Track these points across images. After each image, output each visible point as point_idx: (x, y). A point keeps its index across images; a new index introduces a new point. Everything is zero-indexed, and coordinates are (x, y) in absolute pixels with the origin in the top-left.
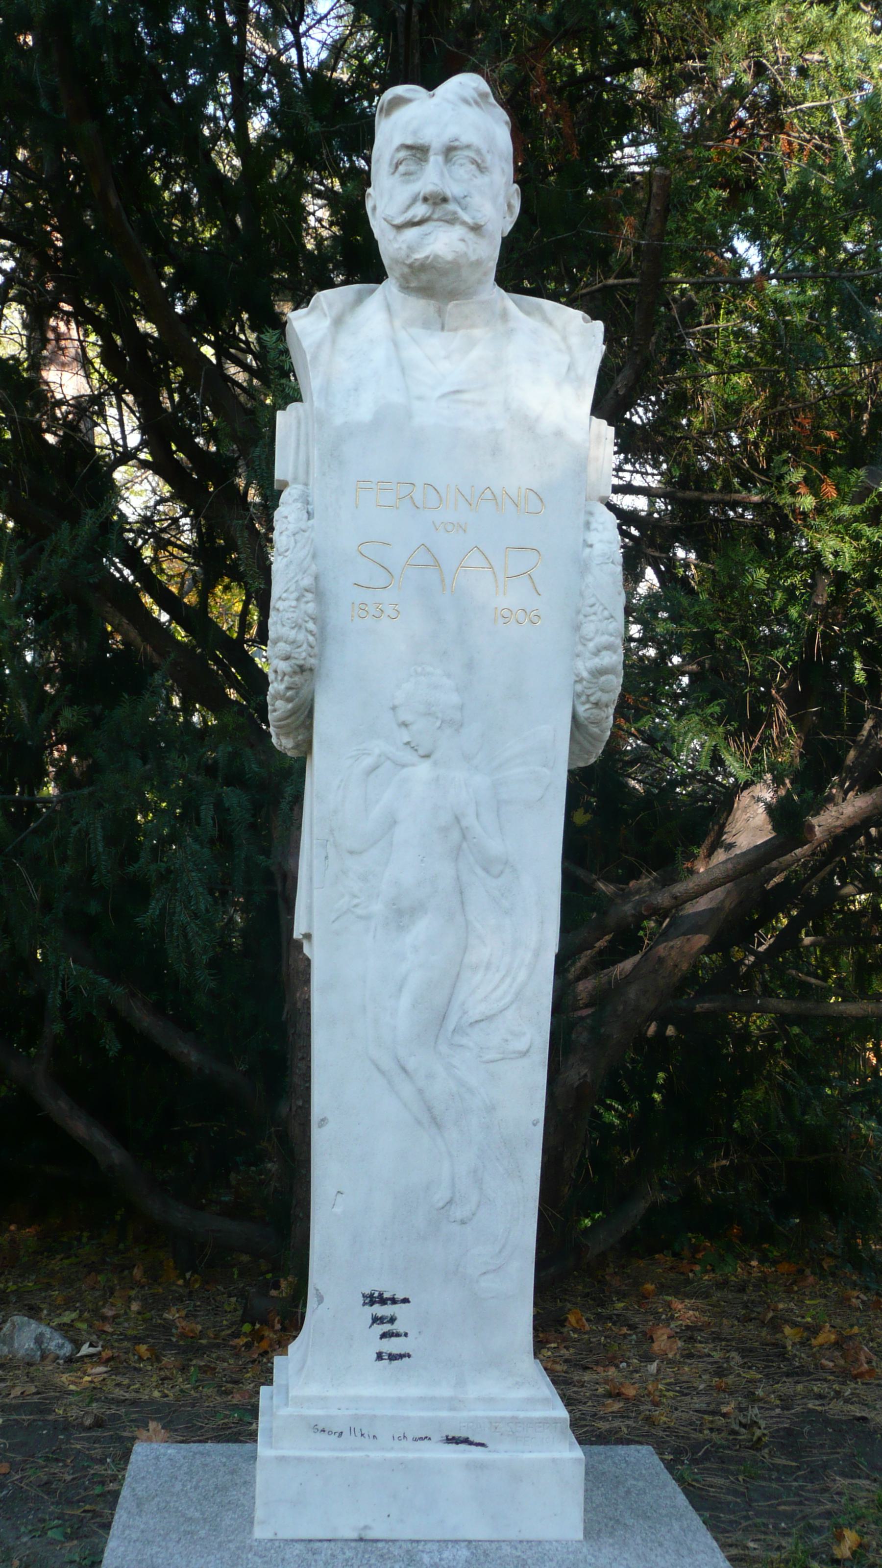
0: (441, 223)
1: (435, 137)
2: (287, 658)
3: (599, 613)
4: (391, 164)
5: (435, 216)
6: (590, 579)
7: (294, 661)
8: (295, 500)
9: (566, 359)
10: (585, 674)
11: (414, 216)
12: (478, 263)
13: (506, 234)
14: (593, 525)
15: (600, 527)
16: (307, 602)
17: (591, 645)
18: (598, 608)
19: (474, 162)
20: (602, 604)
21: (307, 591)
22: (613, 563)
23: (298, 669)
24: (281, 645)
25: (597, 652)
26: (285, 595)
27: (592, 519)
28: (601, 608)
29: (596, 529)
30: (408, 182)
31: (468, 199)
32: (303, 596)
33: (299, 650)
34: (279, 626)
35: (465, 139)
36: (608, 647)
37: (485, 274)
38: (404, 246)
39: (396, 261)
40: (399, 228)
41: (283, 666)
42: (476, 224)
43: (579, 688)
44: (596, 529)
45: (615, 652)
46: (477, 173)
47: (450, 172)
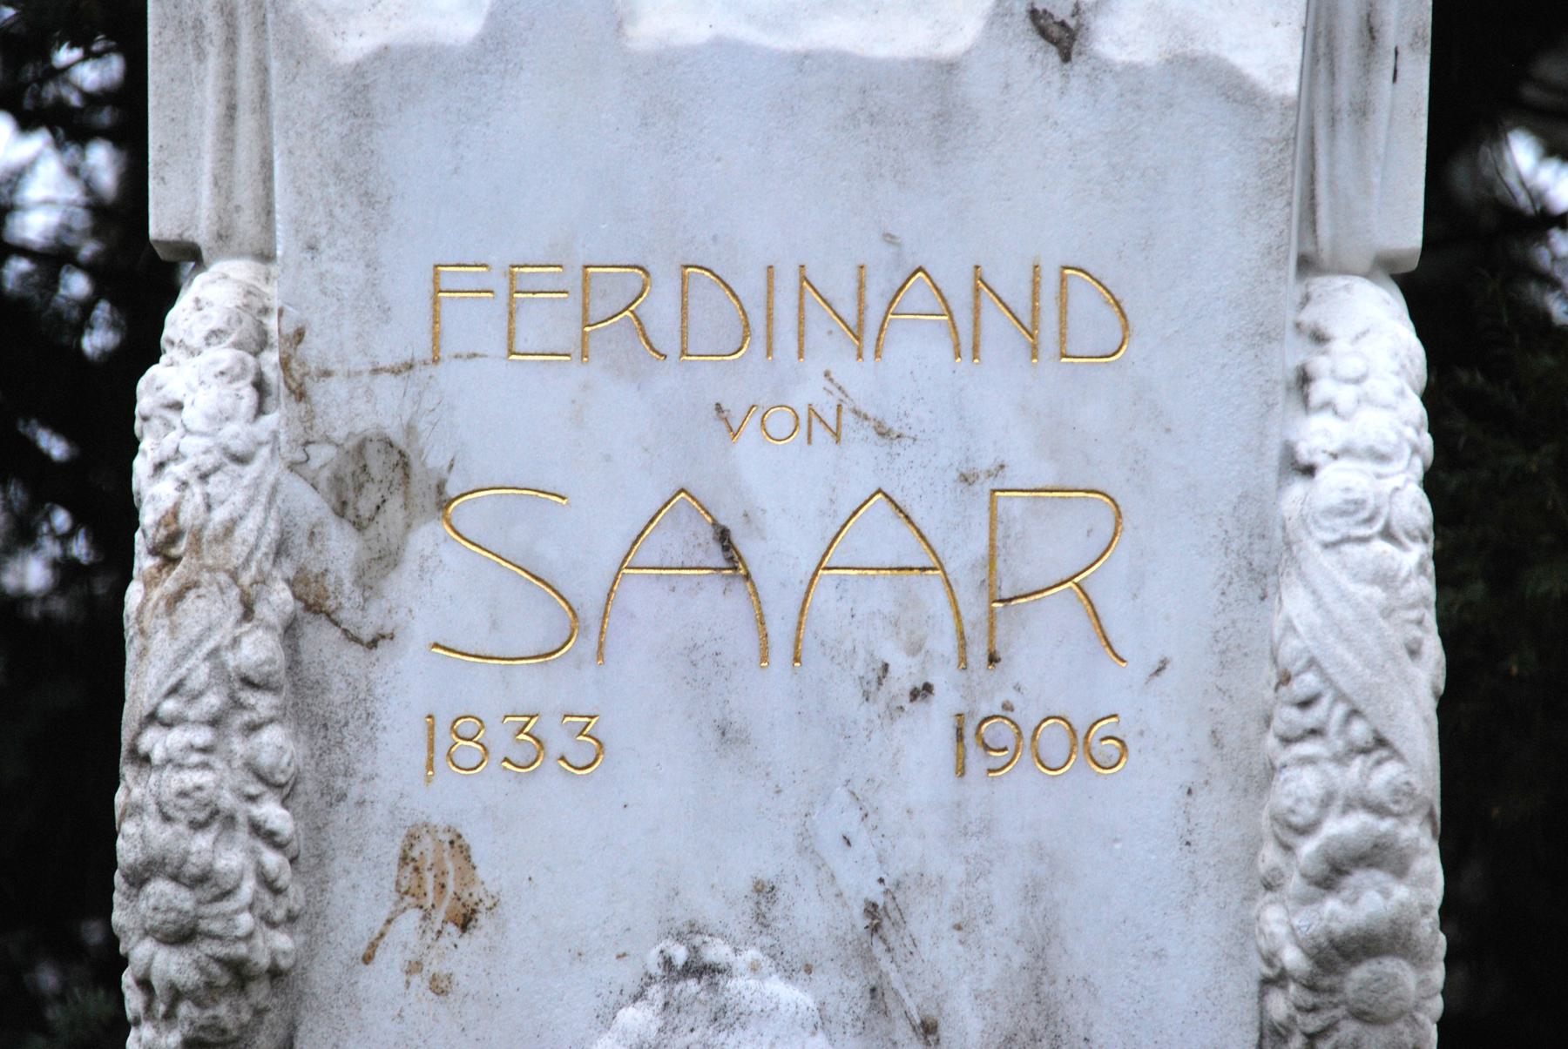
2: (182, 936)
3: (1333, 726)
6: (1296, 603)
7: (209, 948)
8: (215, 335)
10: (1292, 957)
14: (1321, 390)
15: (1345, 396)
16: (253, 728)
17: (1308, 848)
18: (1327, 712)
20: (1340, 696)
21: (248, 682)
22: (1388, 534)
23: (224, 979)
24: (160, 888)
25: (1333, 873)
26: (169, 707)
27: (1320, 364)
28: (1340, 710)
29: (1328, 405)
32: (238, 705)
33: (228, 906)
34: (152, 825)
36: (1377, 856)
41: (171, 965)
43: (1279, 1005)
44: (1328, 405)
45: (1400, 870)
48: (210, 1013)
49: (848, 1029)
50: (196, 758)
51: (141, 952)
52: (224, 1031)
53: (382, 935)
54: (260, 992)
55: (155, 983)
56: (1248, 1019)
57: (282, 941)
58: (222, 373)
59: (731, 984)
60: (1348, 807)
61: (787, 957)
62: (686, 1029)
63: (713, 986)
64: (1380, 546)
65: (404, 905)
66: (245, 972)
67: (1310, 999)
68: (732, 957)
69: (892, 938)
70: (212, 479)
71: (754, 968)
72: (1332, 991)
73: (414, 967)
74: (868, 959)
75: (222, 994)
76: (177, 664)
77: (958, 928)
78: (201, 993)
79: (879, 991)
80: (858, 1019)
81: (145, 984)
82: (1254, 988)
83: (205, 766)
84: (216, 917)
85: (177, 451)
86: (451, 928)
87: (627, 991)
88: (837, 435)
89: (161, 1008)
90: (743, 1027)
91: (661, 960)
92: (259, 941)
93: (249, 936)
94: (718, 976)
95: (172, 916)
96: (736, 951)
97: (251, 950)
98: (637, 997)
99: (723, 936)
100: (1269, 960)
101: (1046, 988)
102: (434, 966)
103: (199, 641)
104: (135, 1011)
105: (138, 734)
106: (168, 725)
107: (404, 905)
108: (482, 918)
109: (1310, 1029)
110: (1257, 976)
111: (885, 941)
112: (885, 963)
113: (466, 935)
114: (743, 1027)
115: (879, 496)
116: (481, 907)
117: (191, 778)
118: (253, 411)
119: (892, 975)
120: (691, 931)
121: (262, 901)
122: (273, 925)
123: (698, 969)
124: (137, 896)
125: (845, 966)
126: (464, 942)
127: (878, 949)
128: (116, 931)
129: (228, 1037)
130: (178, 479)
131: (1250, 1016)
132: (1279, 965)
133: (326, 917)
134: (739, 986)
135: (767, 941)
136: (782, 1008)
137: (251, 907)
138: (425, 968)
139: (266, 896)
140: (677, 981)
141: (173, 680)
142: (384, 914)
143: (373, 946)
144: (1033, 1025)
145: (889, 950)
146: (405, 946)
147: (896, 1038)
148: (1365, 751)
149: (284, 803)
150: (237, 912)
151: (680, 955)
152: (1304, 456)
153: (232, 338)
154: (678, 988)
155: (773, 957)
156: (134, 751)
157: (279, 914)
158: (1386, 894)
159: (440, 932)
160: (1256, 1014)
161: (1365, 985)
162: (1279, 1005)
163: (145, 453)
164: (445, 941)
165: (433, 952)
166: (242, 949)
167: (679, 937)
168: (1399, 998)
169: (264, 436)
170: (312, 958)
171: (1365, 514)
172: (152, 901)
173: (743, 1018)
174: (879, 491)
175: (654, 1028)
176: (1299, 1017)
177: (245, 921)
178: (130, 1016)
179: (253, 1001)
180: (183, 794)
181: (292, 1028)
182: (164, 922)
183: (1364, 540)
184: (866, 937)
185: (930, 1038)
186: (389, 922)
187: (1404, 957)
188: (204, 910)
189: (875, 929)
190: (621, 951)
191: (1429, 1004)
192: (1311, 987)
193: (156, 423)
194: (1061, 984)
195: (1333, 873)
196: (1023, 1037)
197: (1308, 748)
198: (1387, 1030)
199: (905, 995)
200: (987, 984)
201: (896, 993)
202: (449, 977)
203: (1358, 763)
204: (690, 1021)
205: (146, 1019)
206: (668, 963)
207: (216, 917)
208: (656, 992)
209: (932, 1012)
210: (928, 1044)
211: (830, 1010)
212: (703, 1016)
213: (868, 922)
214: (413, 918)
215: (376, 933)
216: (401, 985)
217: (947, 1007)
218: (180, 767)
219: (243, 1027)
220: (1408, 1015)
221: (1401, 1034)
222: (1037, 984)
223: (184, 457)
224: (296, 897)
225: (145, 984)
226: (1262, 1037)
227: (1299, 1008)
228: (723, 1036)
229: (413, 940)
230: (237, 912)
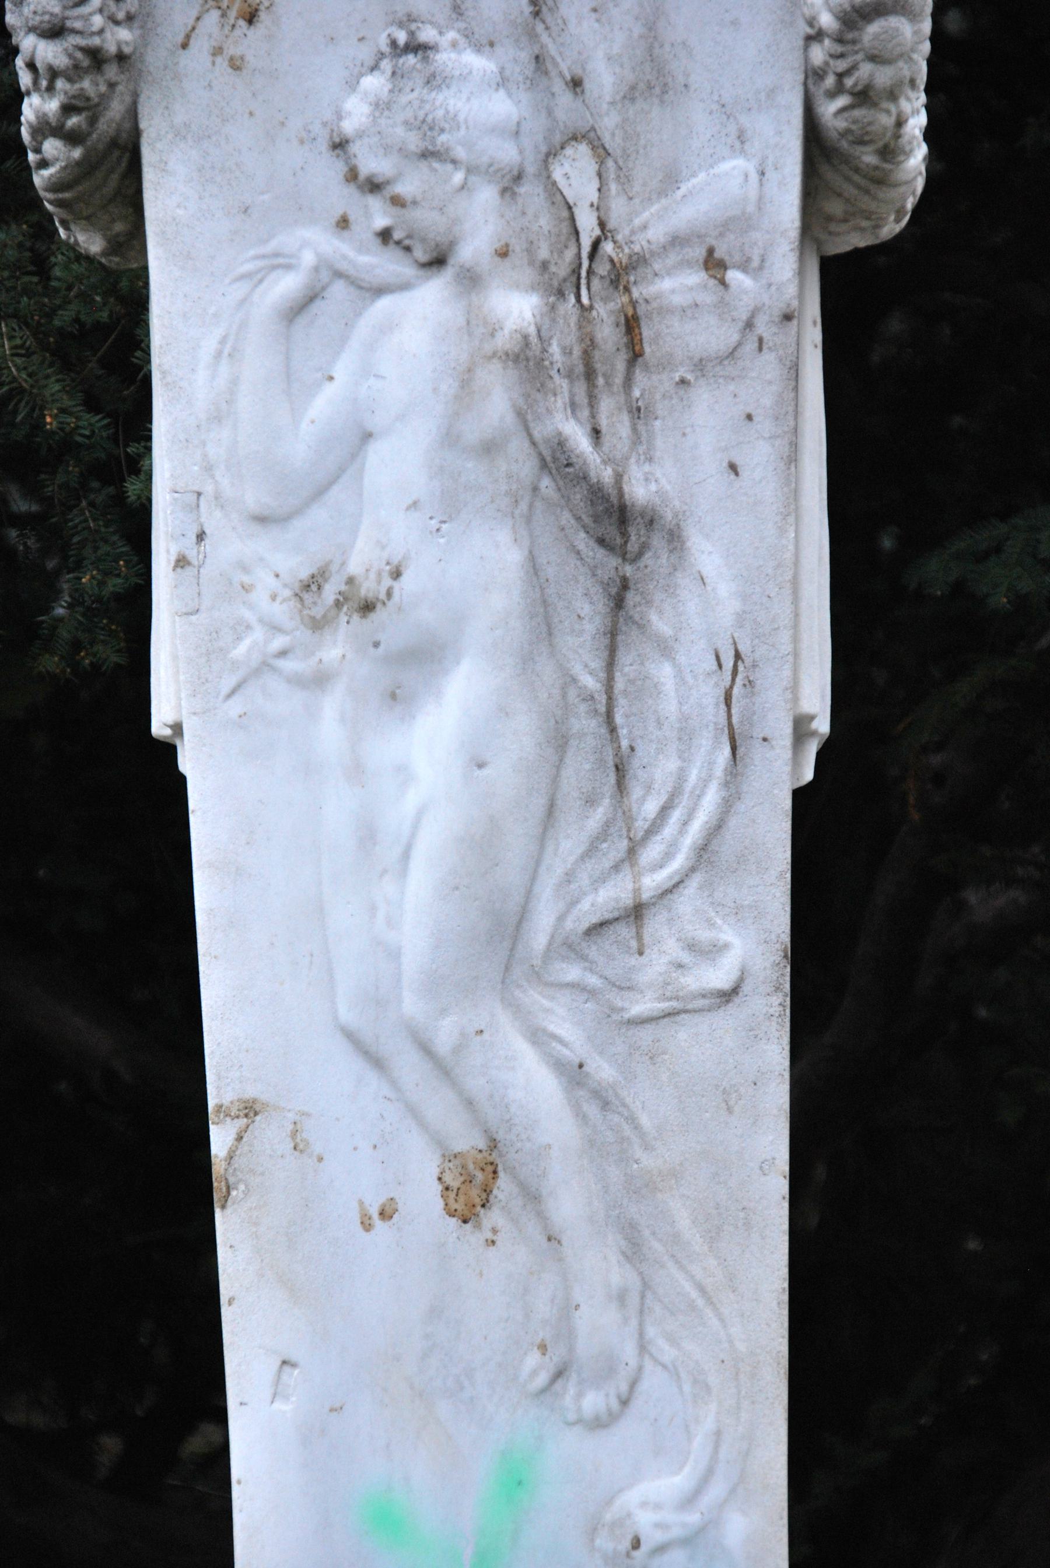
2: (55, 32)
10: (827, 20)
23: (86, 63)
41: (51, 53)
43: (818, 55)
48: (77, 86)
49: (521, 86)
51: (27, 43)
52: (88, 99)
53: (194, 28)
54: (111, 71)
55: (39, 65)
56: (797, 65)
57: (124, 34)
59: (438, 57)
61: (477, 36)
62: (408, 89)
63: (426, 59)
65: (207, 6)
66: (99, 56)
67: (839, 49)
68: (438, 38)
69: (549, 20)
71: (454, 45)
72: (854, 42)
73: (217, 51)
74: (532, 36)
75: (86, 73)
77: (595, 10)
78: (71, 73)
79: (541, 58)
80: (527, 78)
81: (31, 66)
82: (801, 43)
84: (77, 18)
86: (242, 23)
87: (366, 64)
89: (44, 83)
90: (448, 87)
91: (389, 42)
92: (108, 35)
93: (101, 32)
94: (429, 52)
95: (47, 18)
96: (441, 33)
97: (103, 41)
98: (374, 68)
99: (431, 23)
100: (811, 22)
101: (657, 51)
102: (231, 50)
104: (27, 85)
107: (207, 6)
108: (263, 15)
109: (840, 70)
110: (802, 34)
111: (544, 22)
112: (545, 38)
113: (252, 27)
114: (448, 87)
116: (262, 7)
119: (550, 46)
120: (408, 20)
121: (108, 6)
122: (117, 23)
123: (415, 47)
125: (517, 41)
126: (251, 32)
127: (540, 28)
128: (9, 29)
129: (92, 103)
131: (798, 63)
132: (817, 26)
133: (154, 16)
134: (444, 58)
135: (462, 25)
136: (475, 73)
137: (101, 11)
138: (225, 52)
140: (400, 56)
142: (194, 14)
143: (188, 37)
144: (649, 77)
145: (547, 28)
146: (210, 36)
147: (554, 90)
150: (91, 14)
151: (402, 37)
154: (401, 61)
155: (467, 36)
157: (121, 15)
159: (233, 26)
160: (803, 62)
161: (876, 37)
162: (818, 55)
164: (238, 32)
165: (230, 40)
166: (96, 41)
167: (401, 25)
168: (899, 45)
170: (146, 46)
172: (32, 7)
173: (447, 81)
175: (386, 90)
176: (832, 62)
177: (98, 21)
178: (23, 89)
179: (107, 77)
181: (135, 96)
182: (42, 22)
184: (531, 19)
185: (578, 90)
186: (198, 19)
187: (903, 15)
188: (69, 13)
189: (537, 14)
190: (361, 35)
191: (921, 47)
192: (840, 40)
194: (667, 47)
196: (642, 86)
198: (892, 68)
199: (559, 60)
200: (616, 50)
201: (553, 58)
202: (242, 58)
204: (410, 84)
205: (34, 91)
206: (394, 43)
207: (77, 18)
208: (386, 65)
209: (579, 72)
210: (576, 94)
211: (507, 73)
212: (420, 81)
213: (531, 9)
214: (214, 15)
215: (190, 27)
216: (209, 64)
217: (589, 67)
219: (102, 96)
220: (906, 56)
221: (901, 69)
222: (650, 49)
225: (31, 66)
226: (806, 78)
227: (831, 56)
228: (434, 94)
229: (215, 31)
230: (91, 14)
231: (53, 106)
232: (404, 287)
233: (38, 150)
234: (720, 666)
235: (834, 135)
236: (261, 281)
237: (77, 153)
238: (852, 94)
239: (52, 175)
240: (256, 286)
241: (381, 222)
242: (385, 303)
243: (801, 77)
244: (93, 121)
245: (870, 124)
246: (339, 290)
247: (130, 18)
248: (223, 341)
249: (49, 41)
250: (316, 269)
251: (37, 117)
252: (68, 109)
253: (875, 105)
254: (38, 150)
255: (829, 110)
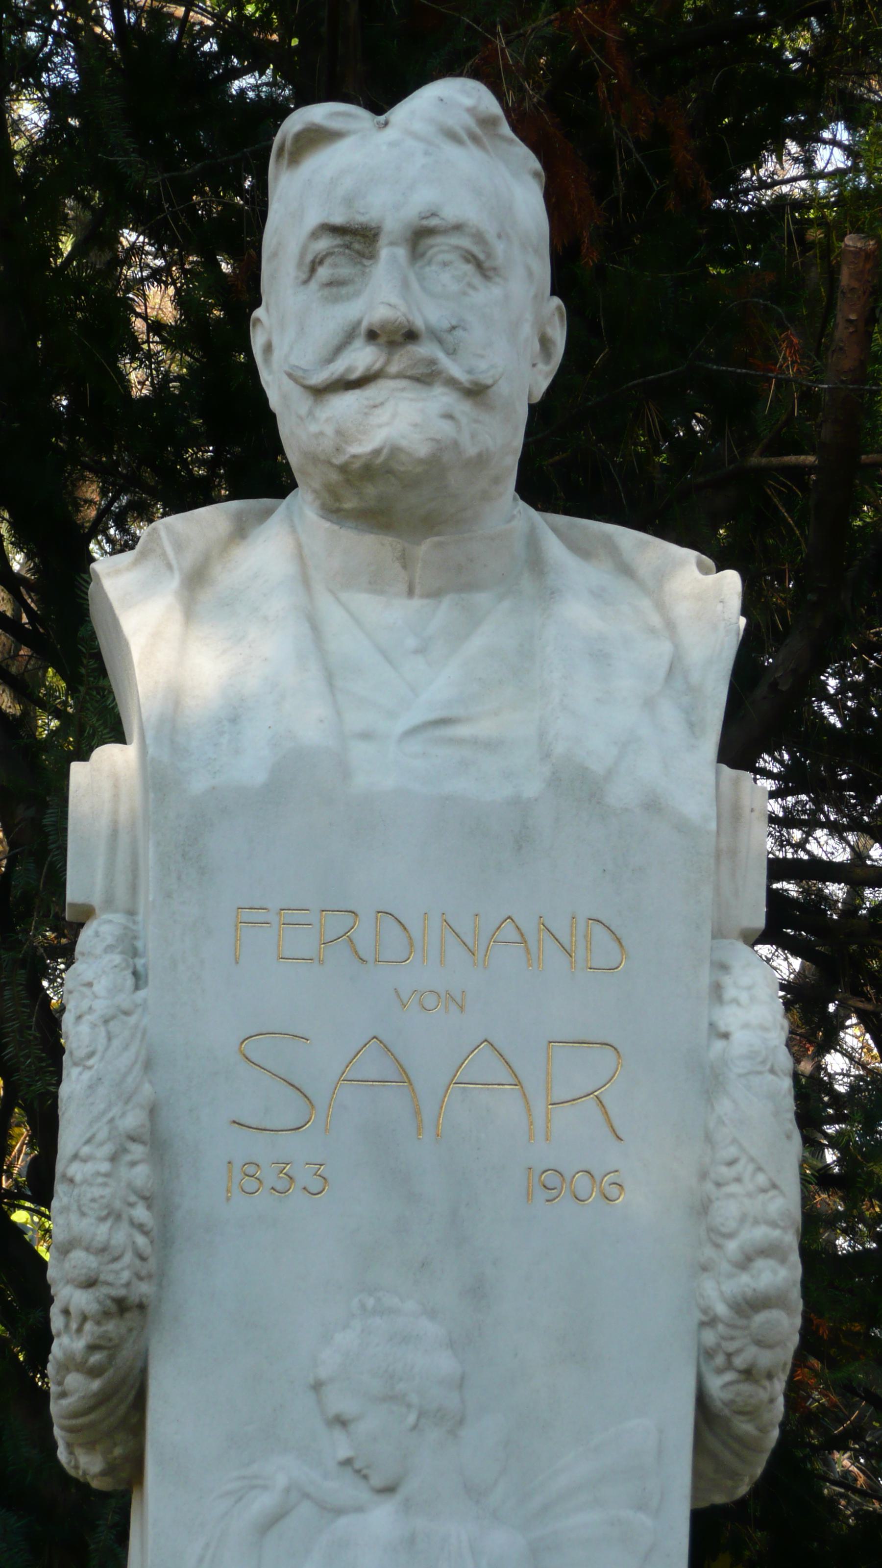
0: (403, 383)
1: (388, 209)
2: (90, 1283)
3: (746, 1178)
4: (300, 264)
5: (393, 369)
7: (104, 1290)
9: (666, 647)
10: (721, 1309)
11: (349, 370)
12: (481, 461)
13: (537, 397)
14: (730, 993)
16: (133, 1164)
17: (732, 1246)
19: (470, 258)
20: (752, 1160)
22: (772, 1071)
23: (113, 1308)
24: (78, 1256)
25: (745, 1262)
26: (86, 1150)
29: (736, 1001)
30: (336, 300)
31: (459, 333)
32: (125, 1150)
33: (116, 1266)
34: (74, 1217)
35: (451, 213)
36: (769, 1251)
37: (497, 480)
38: (329, 430)
39: (314, 459)
40: (320, 392)
42: (476, 383)
43: (710, 1337)
46: (477, 280)
47: (421, 279)
50: (100, 1180)
58: (116, 967)
60: (756, 1222)
64: (770, 1077)
70: (112, 1023)
76: (91, 1125)
81: (66, 1312)
83: (105, 1185)
85: (90, 1008)
88: (462, 1008)
89: (74, 1326)
95: (84, 1271)
103: (104, 1113)
105: (67, 1166)
106: (85, 1160)
115: (485, 1043)
117: (97, 1192)
118: (133, 988)
124: (64, 1260)
130: (91, 1023)
139: (137, 1262)
141: (88, 1135)
148: (764, 1191)
149: (149, 1207)
150: (122, 1269)
152: (723, 1028)
153: (119, 950)
156: (64, 1176)
158: (775, 1272)
163: (70, 1011)
169: (139, 1001)
171: (759, 1059)
174: (486, 1040)
178: (54, 1331)
180: (93, 1200)
183: (760, 1073)
193: (76, 994)
195: (745, 1262)
197: (734, 1188)
203: (761, 1197)
206: (363, 1307)
218: (91, 1185)
223: (95, 1011)
224: (152, 1264)
225: (66, 1312)
231: (79, 1345)
232: (360, 1509)
233: (60, 1383)
234: (423, 218)
235: (719, 1404)
236: (240, 1499)
237: (96, 1385)
238: (740, 1372)
239: (70, 1404)
240: (236, 1502)
241: (344, 1453)
242: (343, 1522)
243: (694, 1354)
244: (111, 1358)
245: (751, 1396)
246: (306, 1509)
247: (150, 1276)
248: (207, 1545)
249: (84, 1291)
250: (288, 1490)
251: (65, 1354)
252: (92, 1348)
253: (756, 1382)
254: (60, 1383)
255: (716, 1384)
